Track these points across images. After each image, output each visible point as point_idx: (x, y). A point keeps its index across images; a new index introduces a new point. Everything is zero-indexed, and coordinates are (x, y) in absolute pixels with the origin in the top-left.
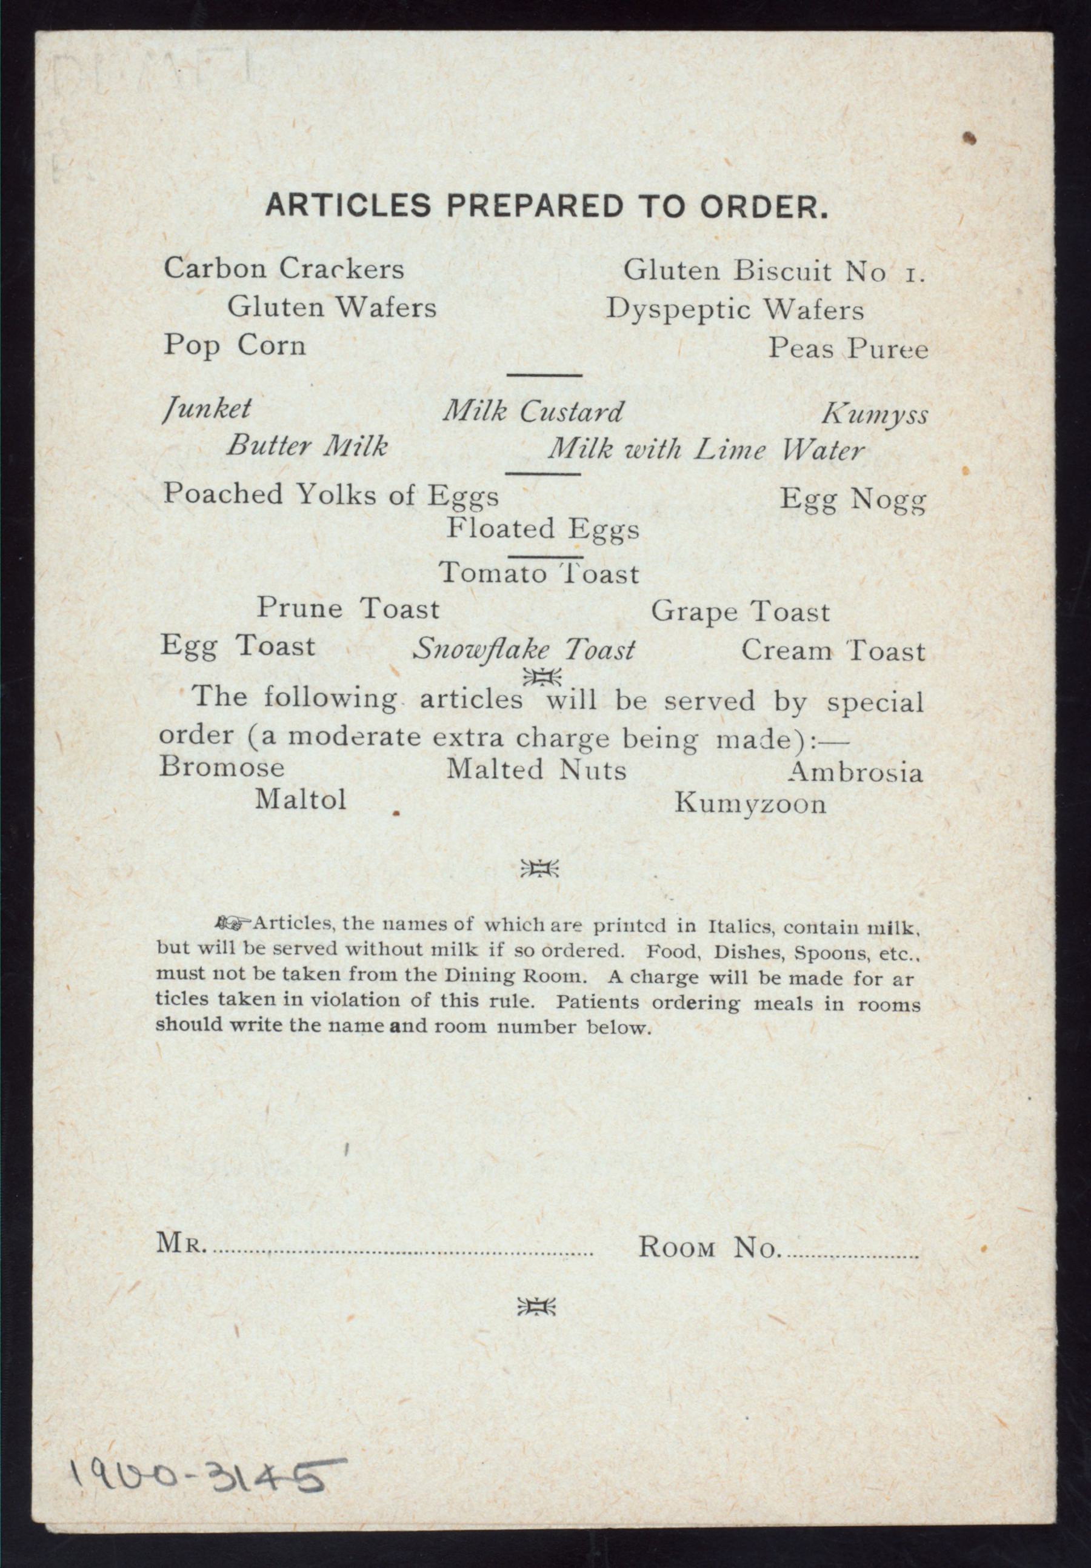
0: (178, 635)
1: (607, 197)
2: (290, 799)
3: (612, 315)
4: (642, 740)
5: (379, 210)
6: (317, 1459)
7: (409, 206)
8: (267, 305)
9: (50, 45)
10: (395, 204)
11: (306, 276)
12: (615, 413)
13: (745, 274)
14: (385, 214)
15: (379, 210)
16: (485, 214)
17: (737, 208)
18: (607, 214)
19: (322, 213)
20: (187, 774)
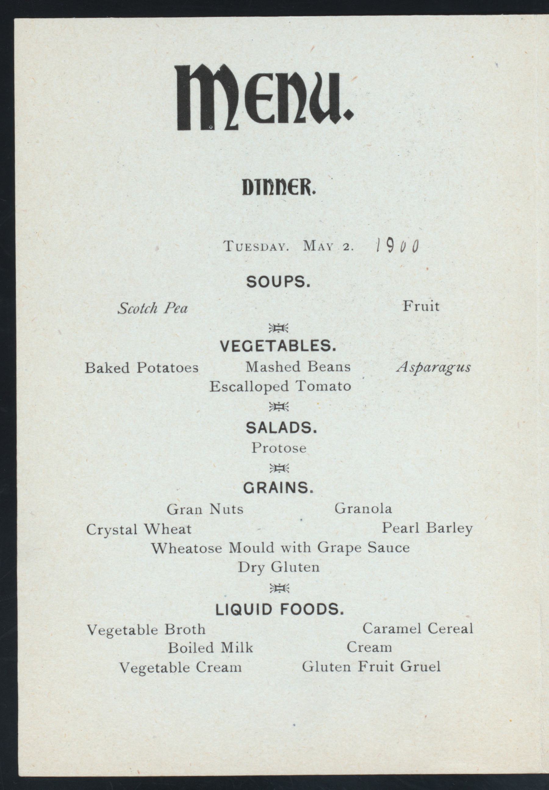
0: (219, 382)
2: (388, 508)
3: (241, 571)
4: (356, 548)
5: (304, 348)
7: (320, 346)
10: (312, 345)
14: (307, 350)
15: (304, 348)
16: (265, 492)
19: (271, 350)
20: (179, 633)
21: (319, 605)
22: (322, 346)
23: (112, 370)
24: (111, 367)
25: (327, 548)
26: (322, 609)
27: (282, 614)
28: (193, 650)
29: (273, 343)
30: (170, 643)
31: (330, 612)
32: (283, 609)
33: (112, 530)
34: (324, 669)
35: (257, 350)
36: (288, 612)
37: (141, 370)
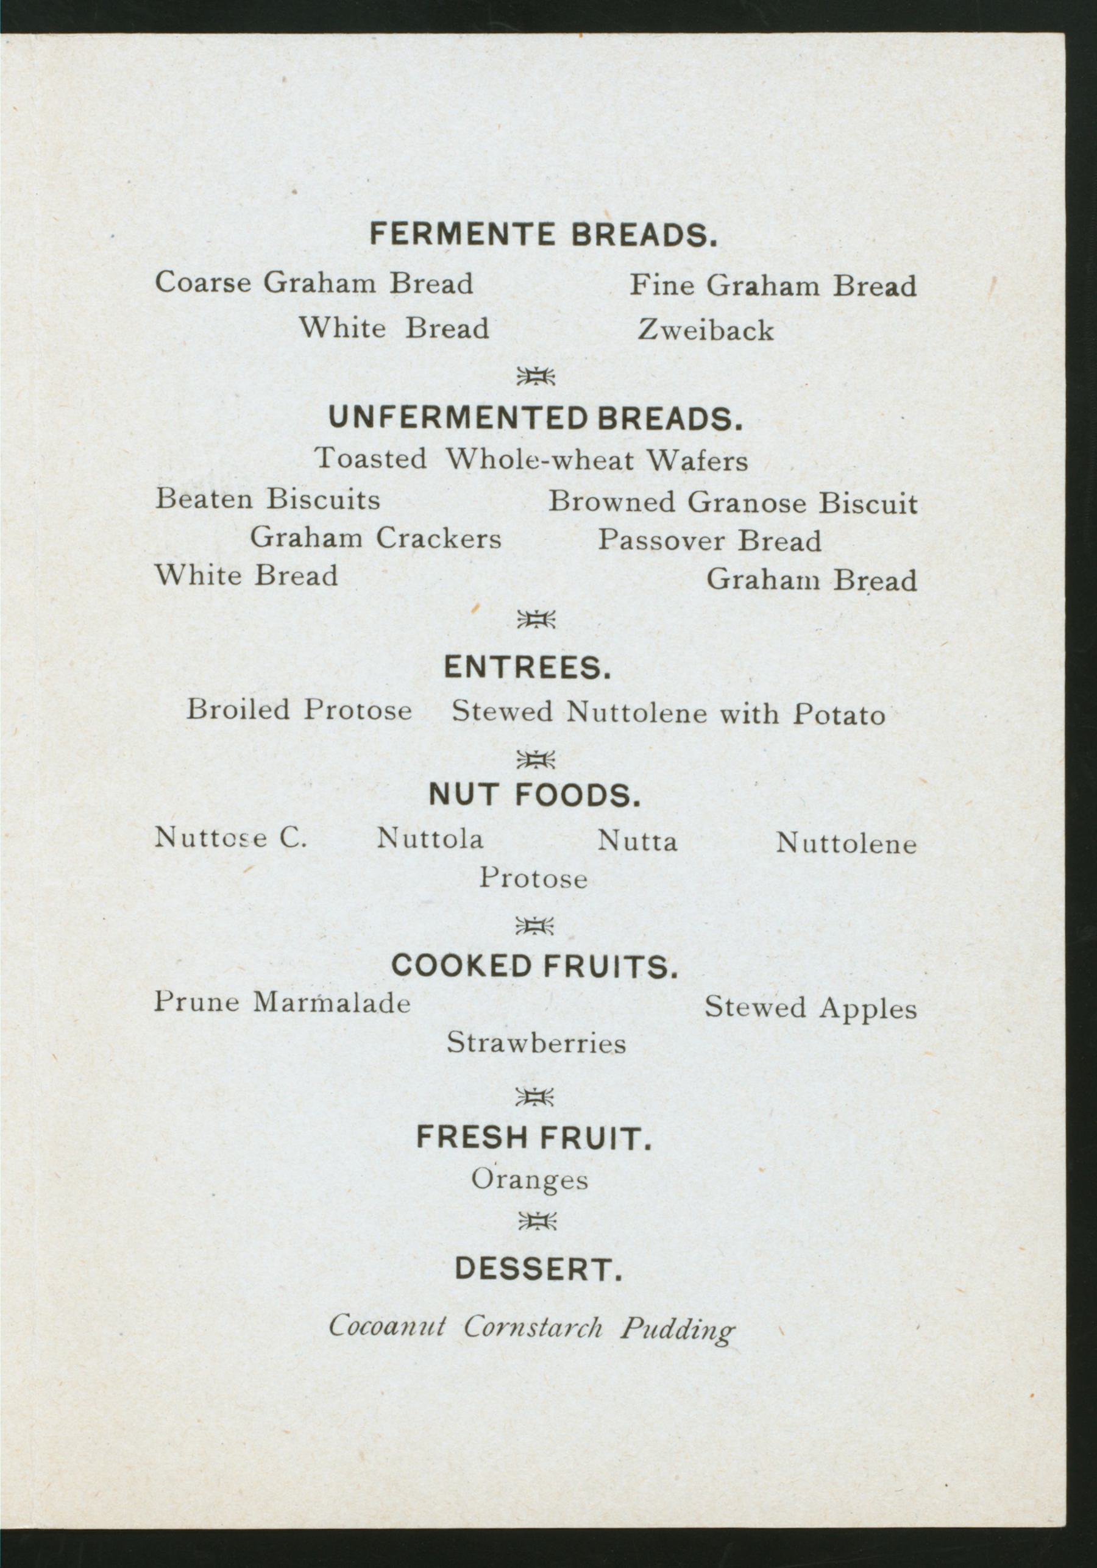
1: (515, 957)
6: (450, 460)
9: (1057, 1518)
11: (402, 545)
12: (667, 1329)
13: (278, 502)
17: (574, 967)
18: (516, 974)
21: (591, 787)
26: (597, 795)
27: (519, 803)
28: (248, 714)
30: (192, 700)
31: (613, 802)
32: (520, 794)
35: (551, 1277)
36: (530, 801)
37: (803, 718)
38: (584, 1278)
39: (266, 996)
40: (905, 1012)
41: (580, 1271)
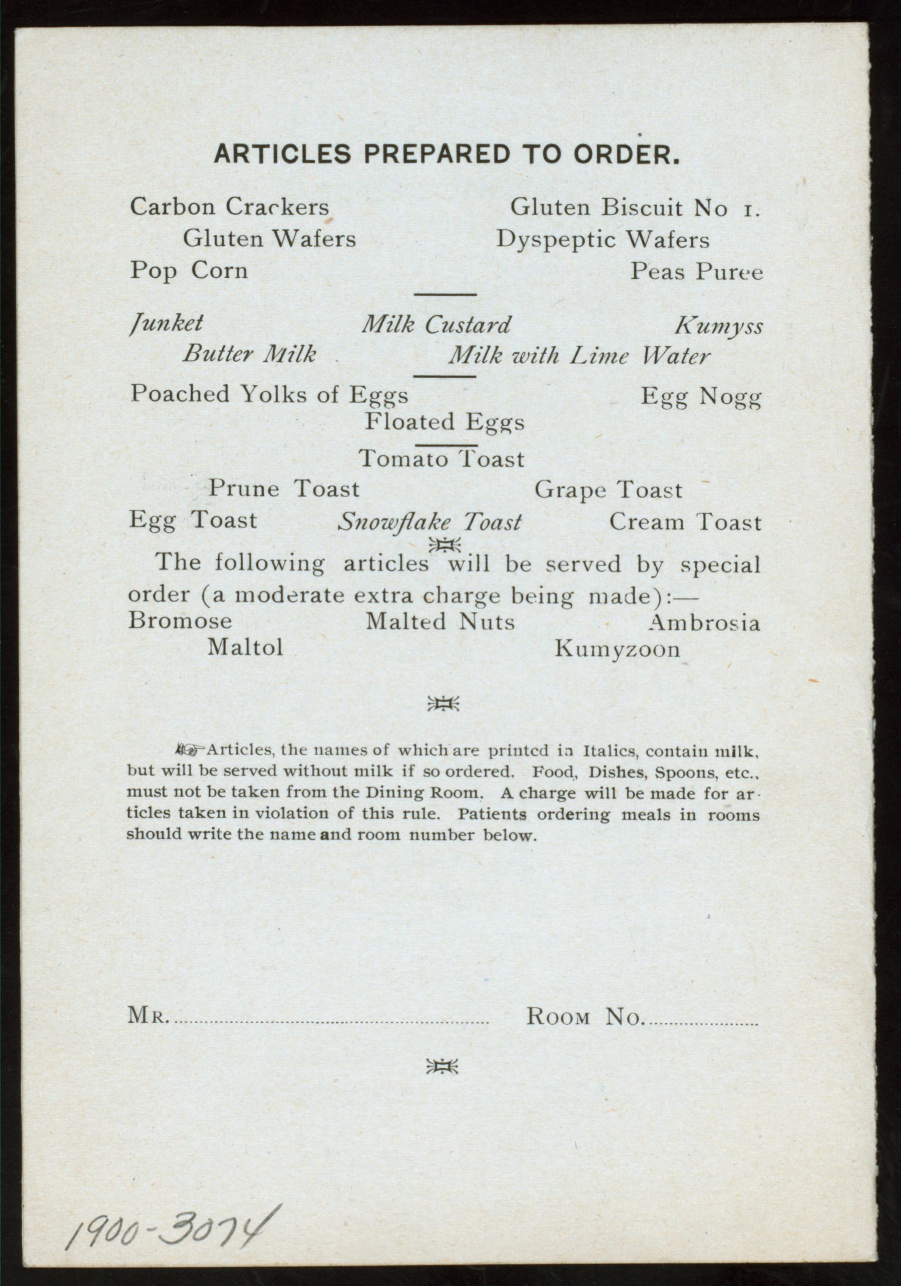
5: (308, 158)
7: (333, 155)
8: (483, 620)
10: (321, 154)
14: (313, 162)
15: (308, 158)
19: (261, 161)
22: (336, 155)
23: (293, 209)
24: (291, 205)
25: (551, 491)
29: (265, 150)
33: (530, 239)
34: (546, 210)
38: (246, 160)
39: (138, 1010)
40: (418, 566)
41: (243, 155)
